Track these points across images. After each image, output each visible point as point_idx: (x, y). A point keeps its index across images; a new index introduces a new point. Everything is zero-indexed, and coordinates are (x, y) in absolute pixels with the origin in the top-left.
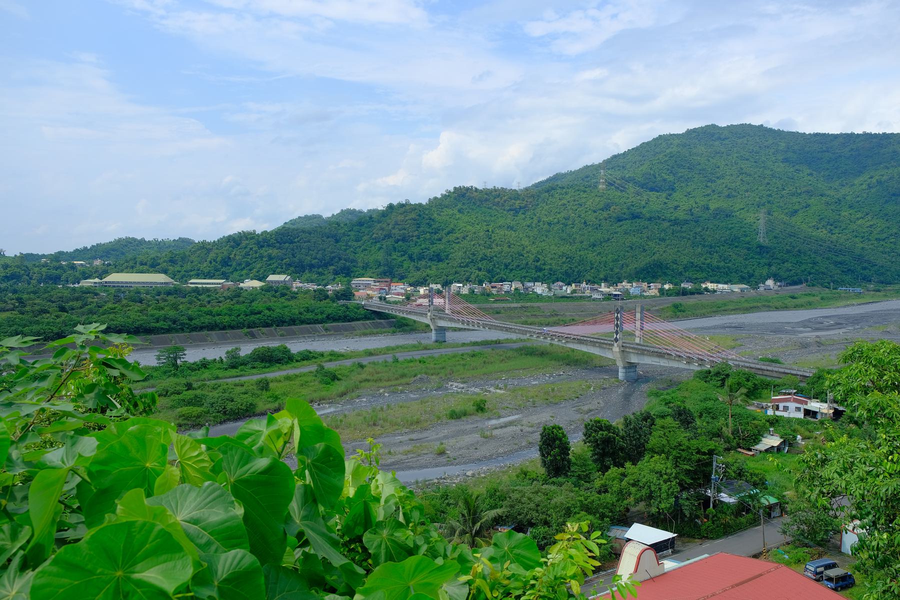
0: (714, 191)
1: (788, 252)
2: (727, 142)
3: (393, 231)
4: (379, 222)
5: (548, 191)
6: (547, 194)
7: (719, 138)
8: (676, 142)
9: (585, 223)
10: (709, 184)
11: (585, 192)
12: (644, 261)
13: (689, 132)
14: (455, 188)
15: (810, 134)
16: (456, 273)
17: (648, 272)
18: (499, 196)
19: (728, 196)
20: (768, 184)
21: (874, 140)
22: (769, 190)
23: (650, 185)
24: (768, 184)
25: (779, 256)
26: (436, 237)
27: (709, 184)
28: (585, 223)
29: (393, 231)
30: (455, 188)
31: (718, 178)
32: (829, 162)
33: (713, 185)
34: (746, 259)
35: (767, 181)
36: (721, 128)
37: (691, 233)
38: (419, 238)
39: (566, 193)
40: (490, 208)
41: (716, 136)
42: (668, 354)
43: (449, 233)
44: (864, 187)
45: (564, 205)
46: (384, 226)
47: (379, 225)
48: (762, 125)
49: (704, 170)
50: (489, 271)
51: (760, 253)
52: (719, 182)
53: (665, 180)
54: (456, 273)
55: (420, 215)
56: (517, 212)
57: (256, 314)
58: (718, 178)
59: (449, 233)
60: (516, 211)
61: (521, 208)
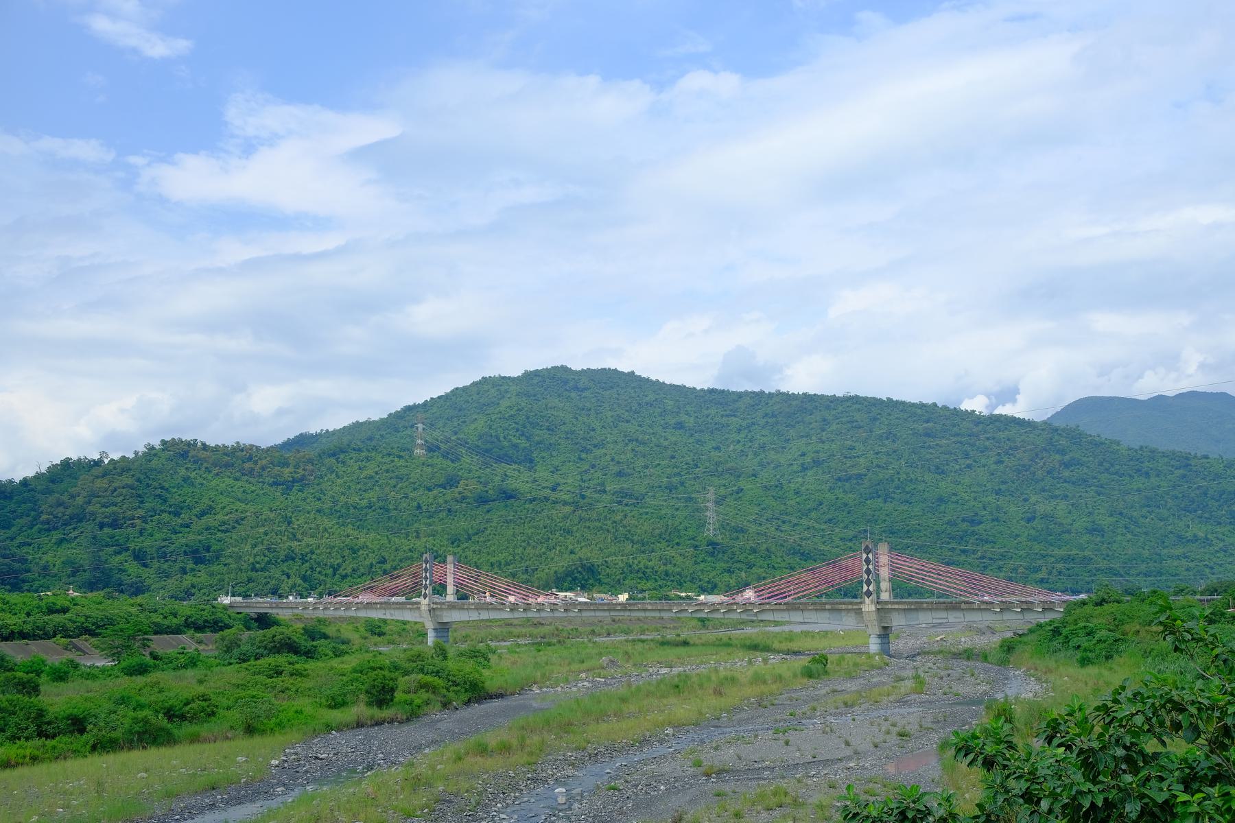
0: (593, 466)
1: (754, 551)
2: (587, 394)
3: (90, 508)
4: (48, 492)
5: (334, 455)
6: (333, 460)
7: (576, 388)
8: (513, 388)
9: (419, 507)
10: (583, 456)
11: (400, 457)
12: (562, 563)
13: (529, 376)
14: (164, 442)
15: (702, 390)
16: (250, 580)
17: (575, 579)
18: (250, 459)
19: (620, 474)
20: (673, 457)
21: (794, 403)
22: (676, 467)
23: (491, 451)
24: (673, 457)
25: (742, 557)
26: (180, 521)
27: (583, 456)
28: (419, 507)
29: (90, 508)
30: (164, 442)
31: (595, 446)
32: (739, 431)
33: (590, 457)
34: (696, 563)
35: (670, 452)
36: (575, 372)
37: (609, 522)
38: (145, 522)
39: (368, 459)
40: (236, 479)
41: (571, 384)
42: (966, 603)
43: (203, 514)
44: (795, 468)
45: (371, 477)
46: (65, 498)
47: (51, 499)
48: (633, 373)
49: (573, 432)
50: (304, 579)
51: (712, 554)
52: (598, 452)
53: (515, 446)
54: (250, 580)
55: (138, 480)
56: (290, 488)
57: (58, 611)
58: (595, 446)
59: (203, 514)
60: (288, 486)
61: (294, 481)
